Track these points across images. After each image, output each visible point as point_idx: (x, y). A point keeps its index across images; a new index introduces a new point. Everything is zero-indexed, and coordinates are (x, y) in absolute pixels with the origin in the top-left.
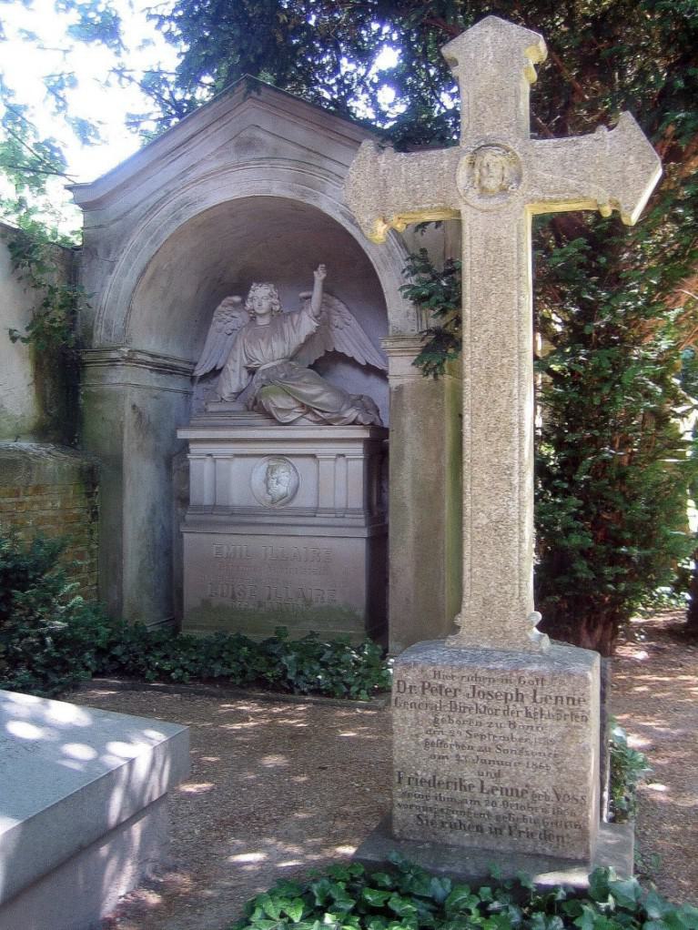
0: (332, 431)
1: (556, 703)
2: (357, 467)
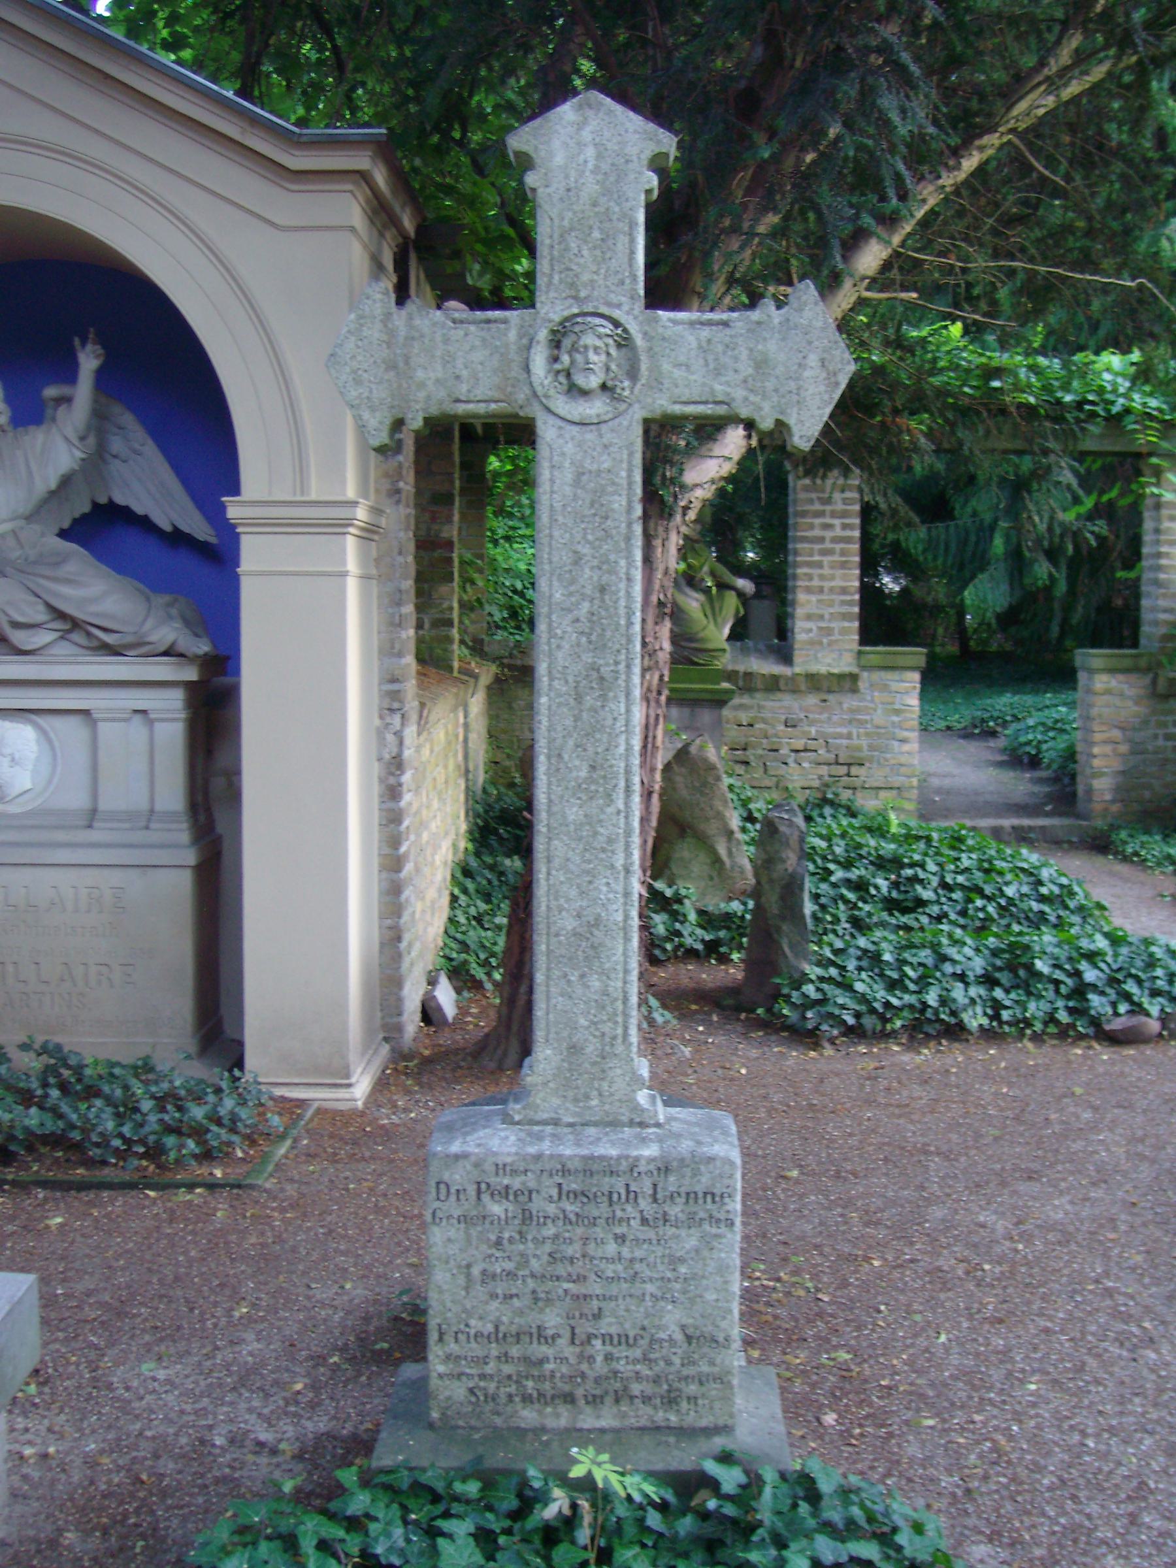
0: (123, 668)
1: (687, 1202)
2: (172, 733)
